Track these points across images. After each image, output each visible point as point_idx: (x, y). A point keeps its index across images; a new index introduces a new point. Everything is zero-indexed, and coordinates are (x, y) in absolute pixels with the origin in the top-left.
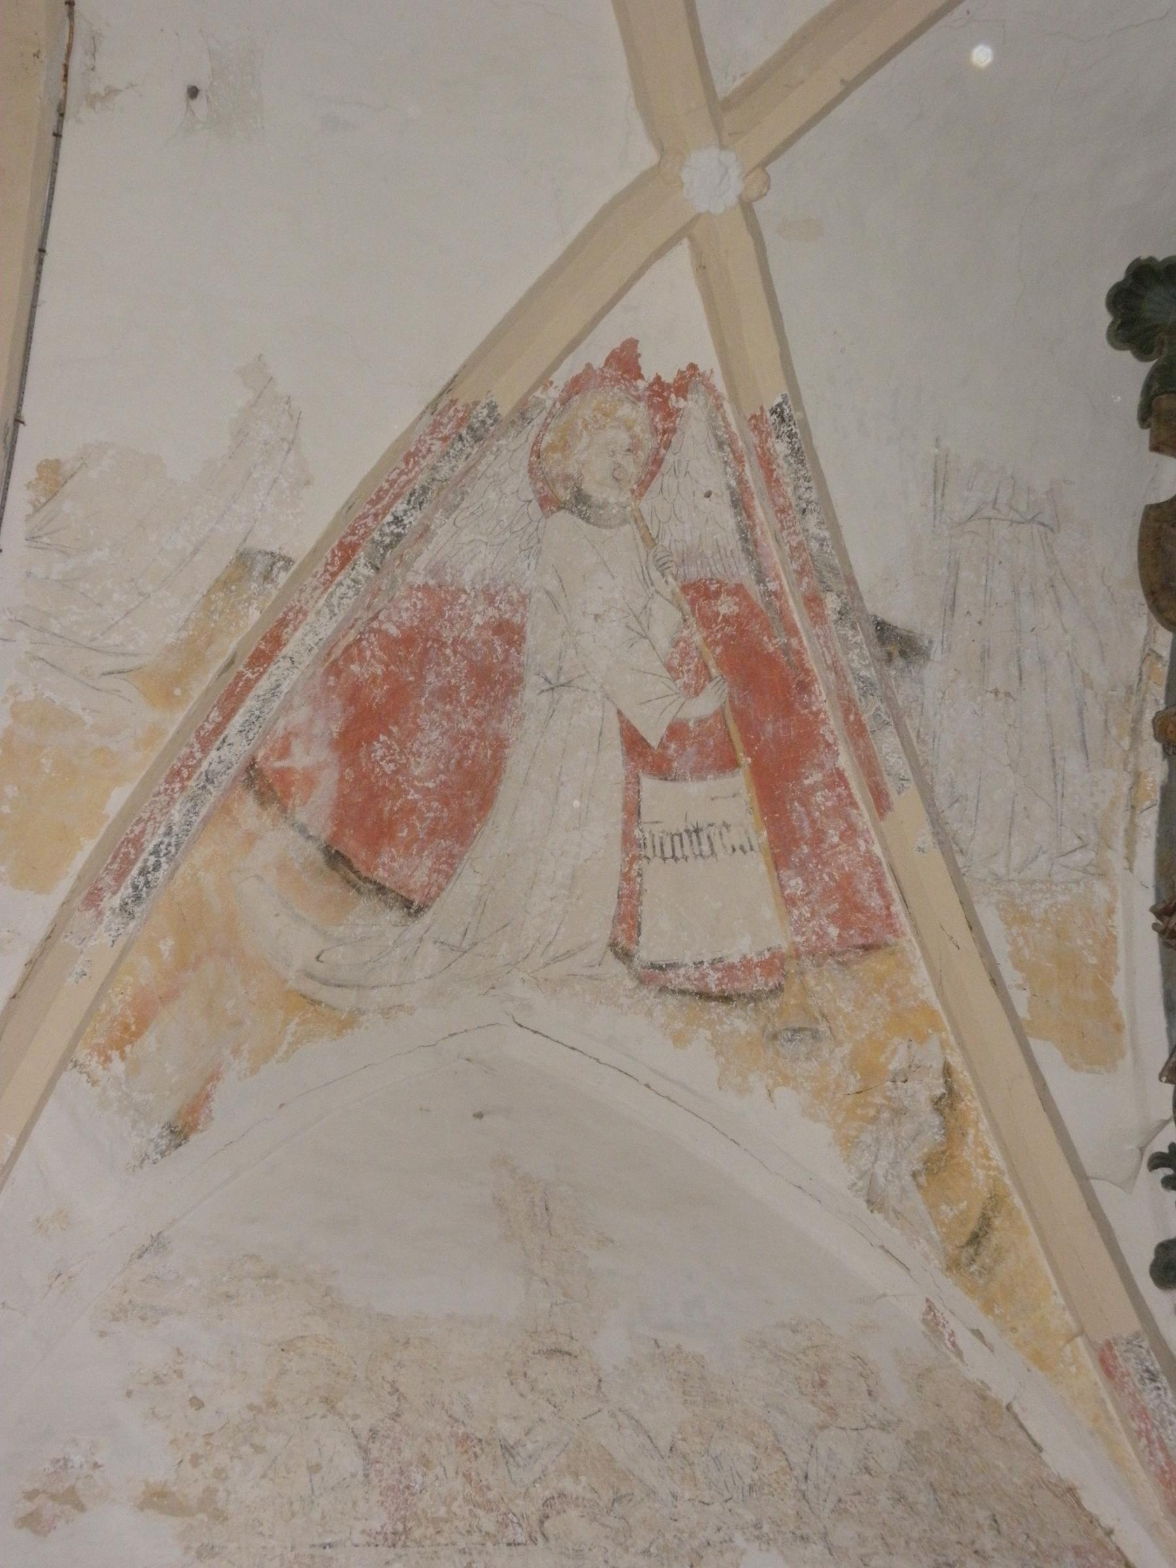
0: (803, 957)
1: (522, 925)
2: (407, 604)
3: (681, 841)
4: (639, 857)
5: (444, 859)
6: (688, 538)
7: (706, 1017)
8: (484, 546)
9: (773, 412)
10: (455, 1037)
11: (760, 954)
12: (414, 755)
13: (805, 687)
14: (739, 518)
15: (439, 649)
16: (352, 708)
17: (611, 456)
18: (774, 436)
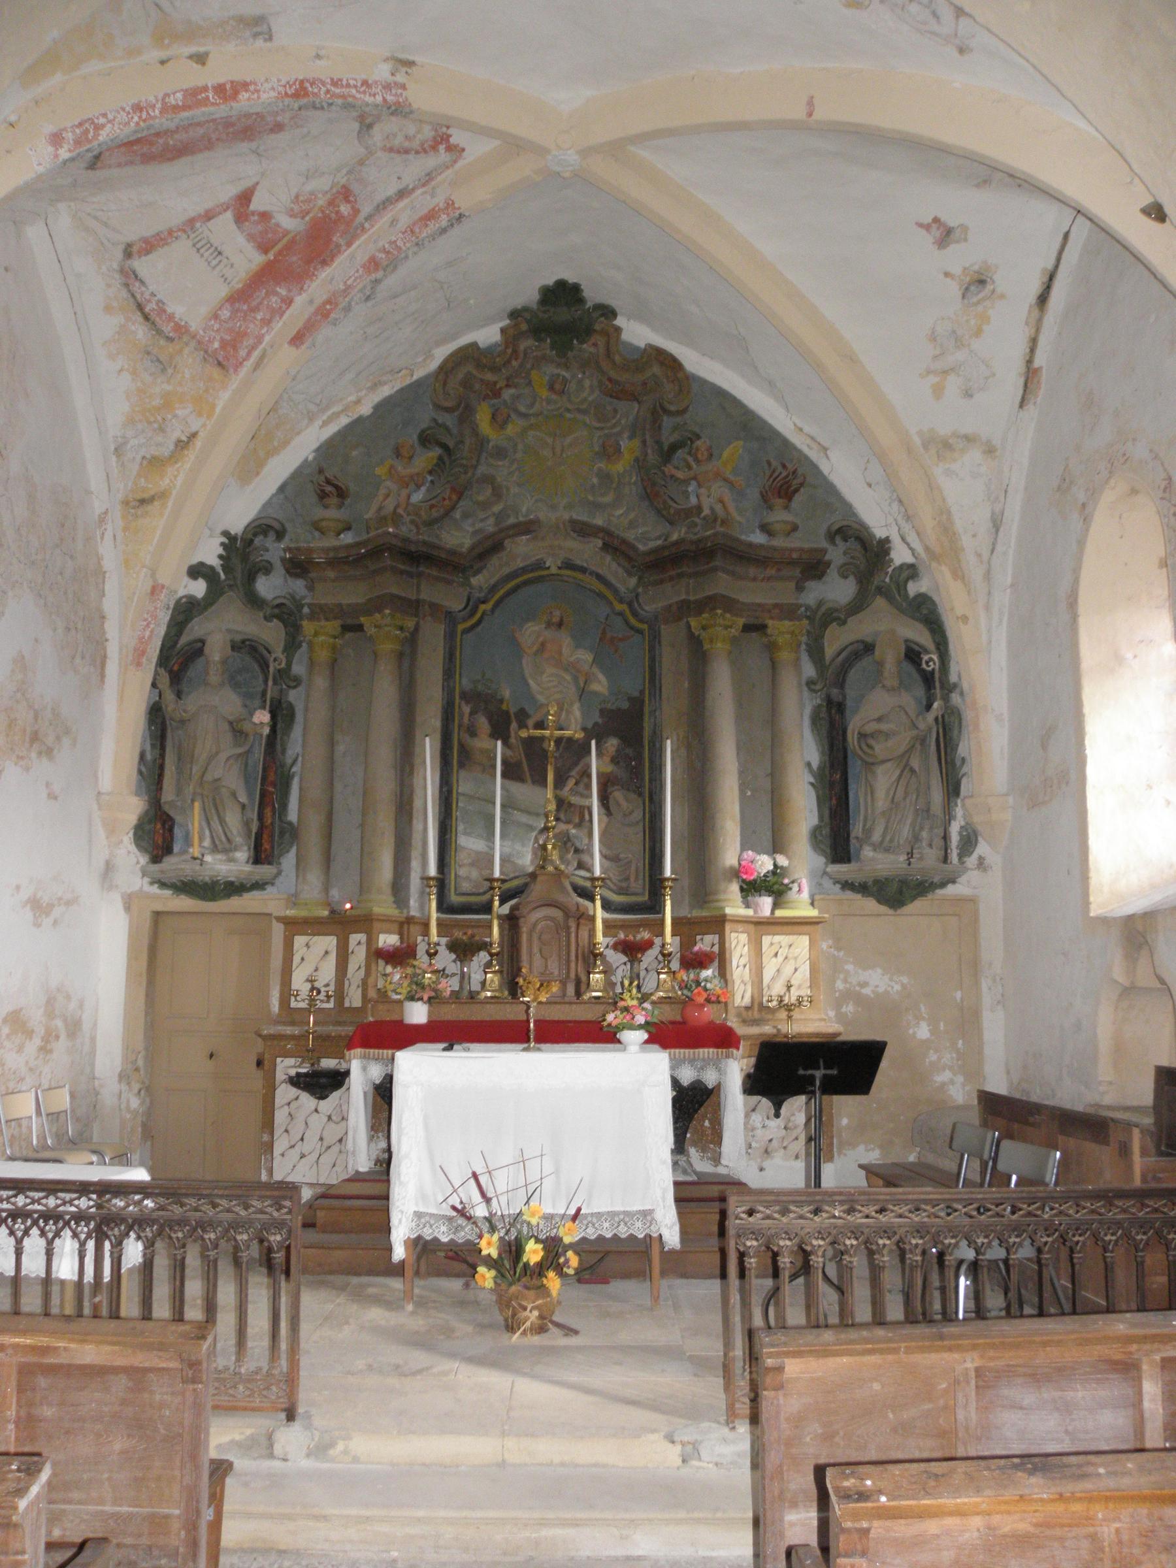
13: (324, 263)
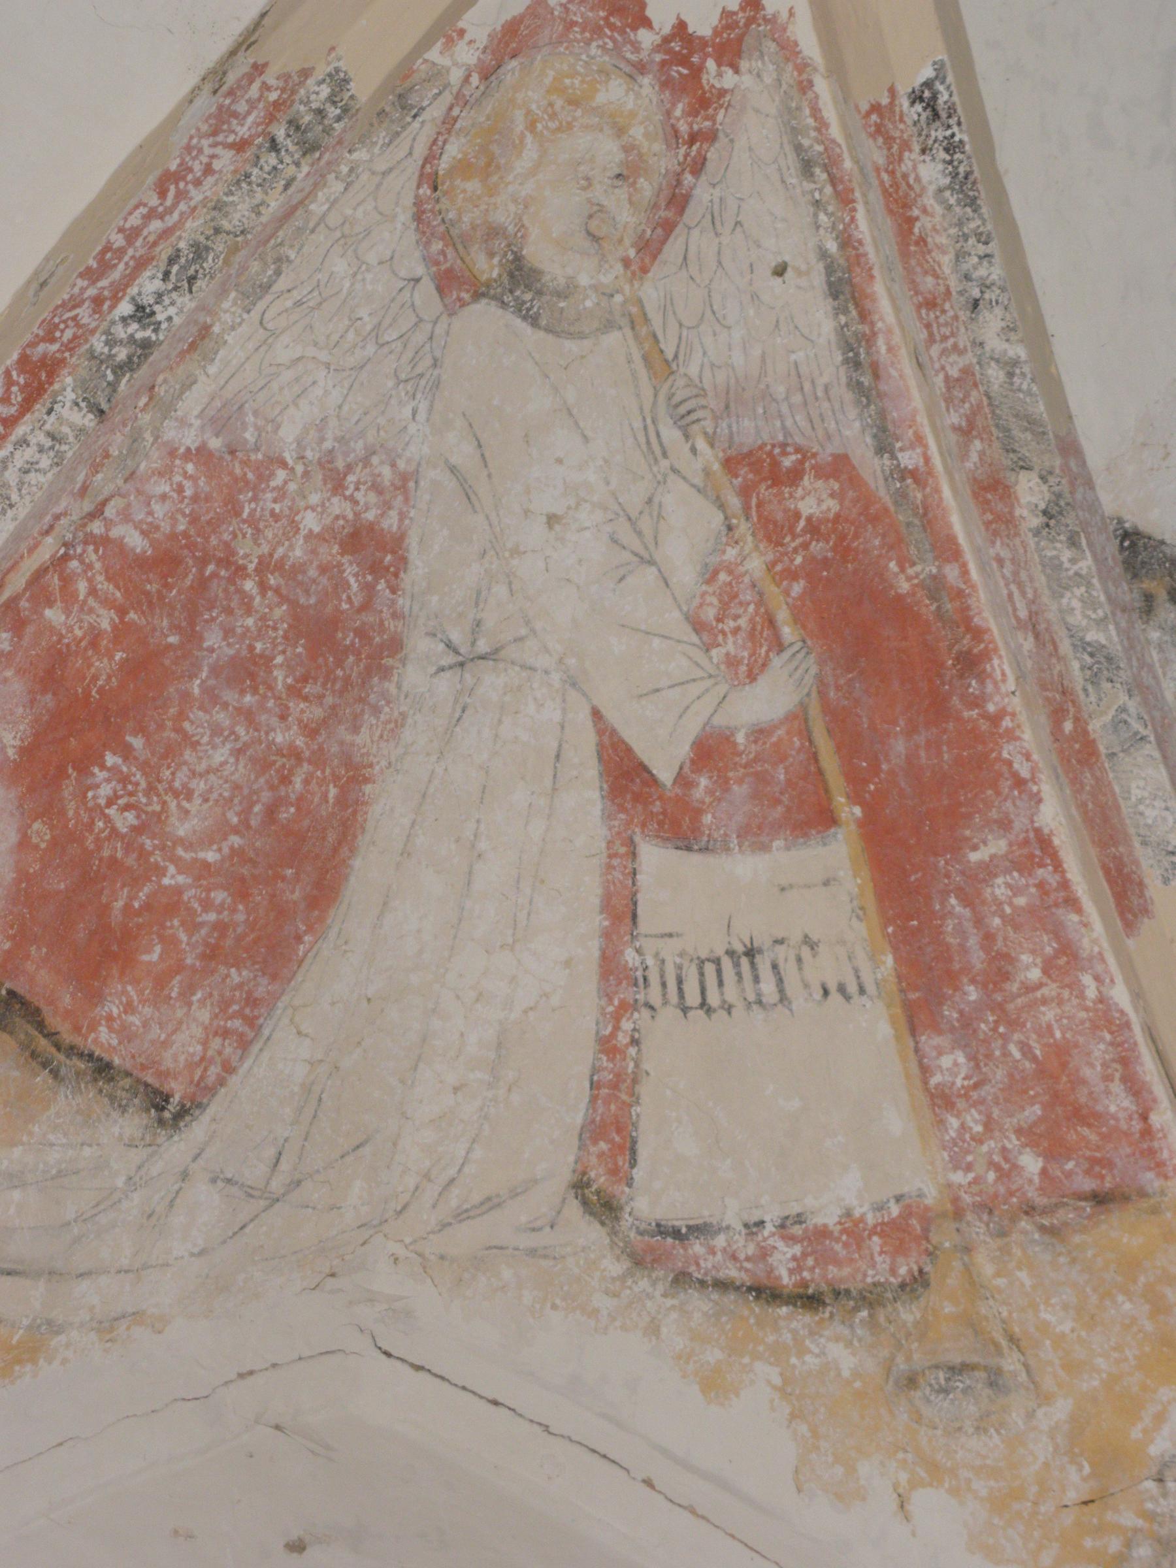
0: (969, 1217)
1: (395, 1144)
2: (164, 487)
3: (719, 972)
4: (635, 1006)
5: (236, 1007)
6: (738, 359)
7: (771, 1339)
8: (323, 373)
9: (916, 98)
10: (250, 1380)
11: (880, 1208)
12: (176, 794)
14: (843, 319)
15: (231, 580)
16: (49, 696)
17: (584, 189)
18: (917, 148)
